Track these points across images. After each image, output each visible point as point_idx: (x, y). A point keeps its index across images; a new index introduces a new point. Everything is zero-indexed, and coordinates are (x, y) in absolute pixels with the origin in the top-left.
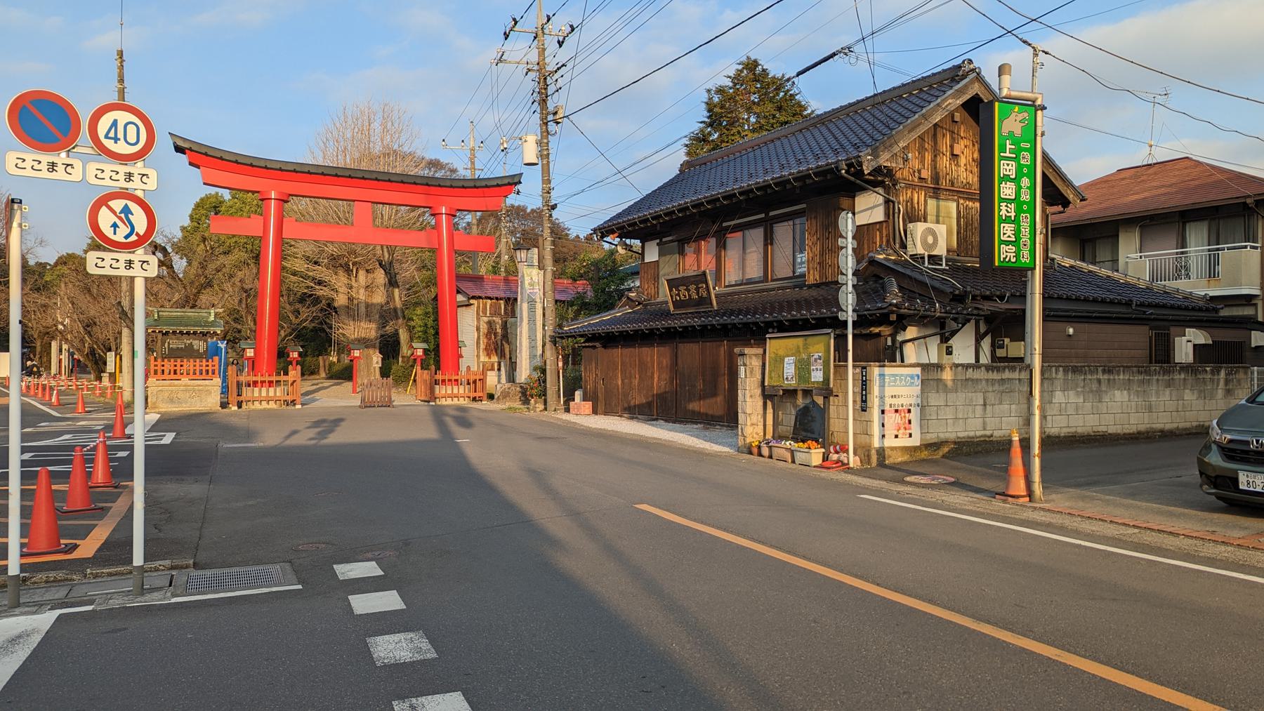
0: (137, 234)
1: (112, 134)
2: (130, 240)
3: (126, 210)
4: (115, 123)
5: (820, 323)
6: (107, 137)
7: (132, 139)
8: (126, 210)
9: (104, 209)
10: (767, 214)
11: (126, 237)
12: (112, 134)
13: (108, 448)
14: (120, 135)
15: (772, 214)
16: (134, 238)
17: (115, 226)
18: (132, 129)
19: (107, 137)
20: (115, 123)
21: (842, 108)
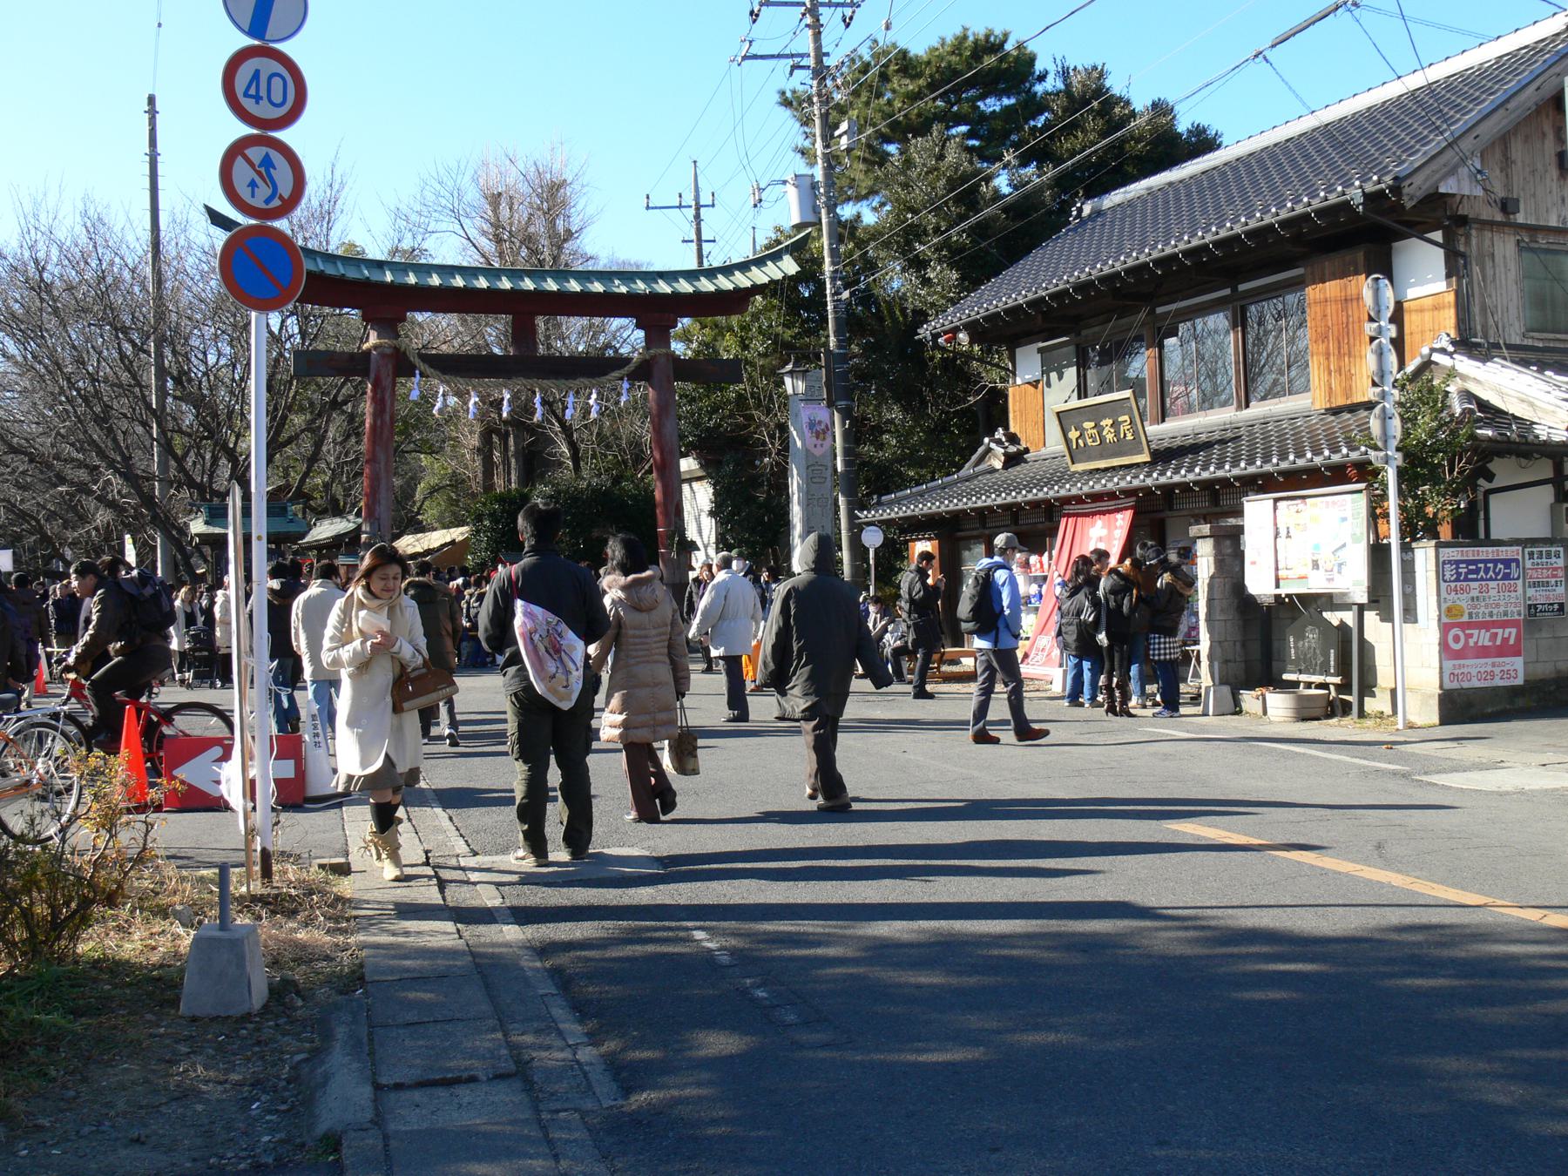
0: (281, 197)
1: (252, 91)
2: (271, 206)
3: (267, 162)
4: (257, 73)
5: (1336, 475)
6: (246, 95)
7: (277, 98)
8: (267, 162)
9: (240, 159)
10: (1234, 289)
11: (267, 201)
12: (252, 91)
13: (1205, 714)
14: (263, 93)
15: (1242, 287)
16: (276, 203)
17: (253, 184)
18: (277, 84)
19: (246, 95)
20: (256, 75)
21: (1285, 147)
